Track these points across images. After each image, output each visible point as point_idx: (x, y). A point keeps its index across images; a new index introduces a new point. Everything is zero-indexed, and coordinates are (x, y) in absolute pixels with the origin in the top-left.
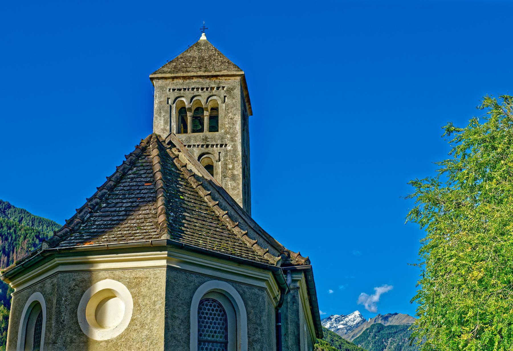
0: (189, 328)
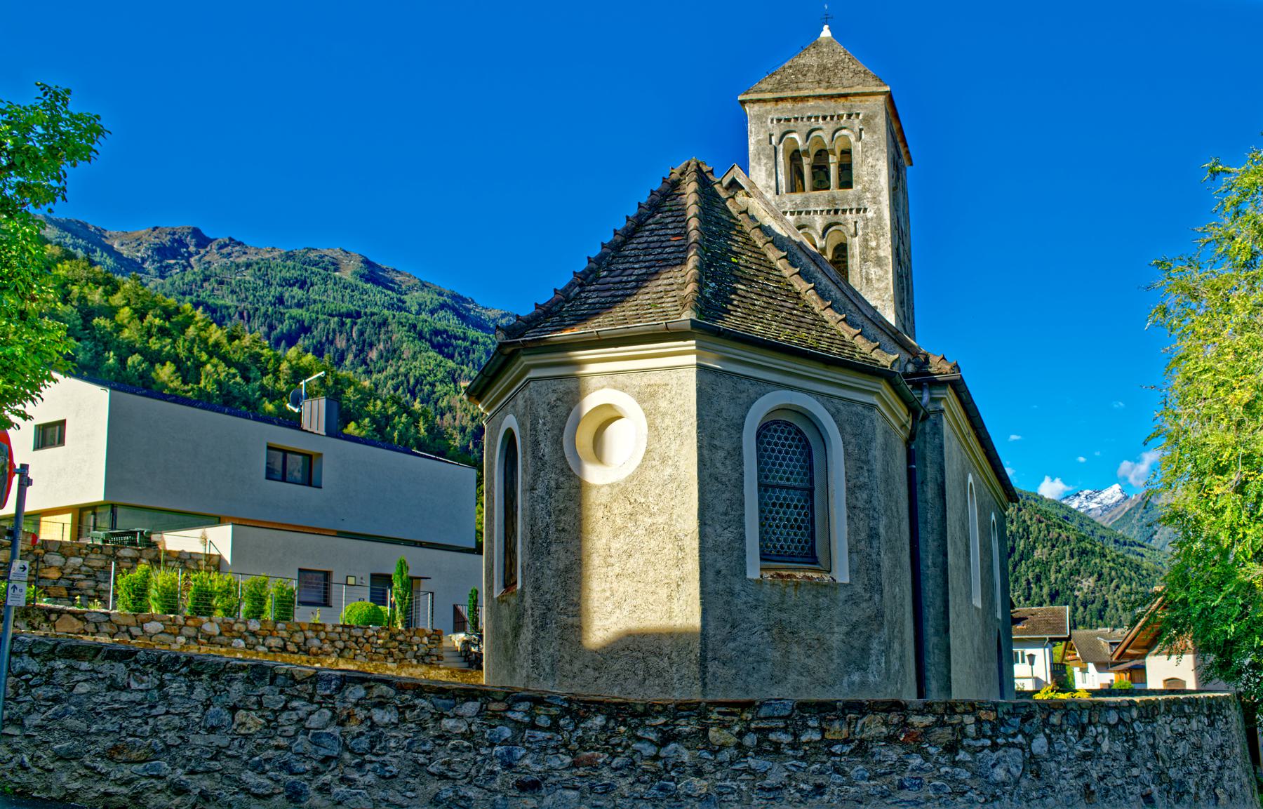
0: (741, 464)
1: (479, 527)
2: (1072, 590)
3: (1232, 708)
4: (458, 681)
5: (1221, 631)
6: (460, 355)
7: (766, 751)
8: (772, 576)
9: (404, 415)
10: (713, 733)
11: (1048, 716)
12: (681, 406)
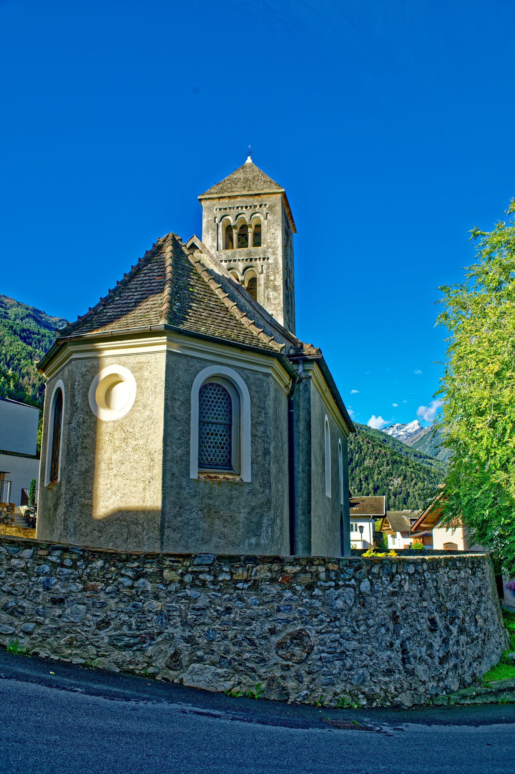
0: (189, 409)
1: (39, 442)
2: (388, 485)
3: (487, 563)
4: (21, 535)
5: (480, 514)
6: (35, 343)
7: (197, 585)
8: (205, 477)
9: (3, 377)
10: (166, 573)
11: (371, 568)
12: (156, 375)
